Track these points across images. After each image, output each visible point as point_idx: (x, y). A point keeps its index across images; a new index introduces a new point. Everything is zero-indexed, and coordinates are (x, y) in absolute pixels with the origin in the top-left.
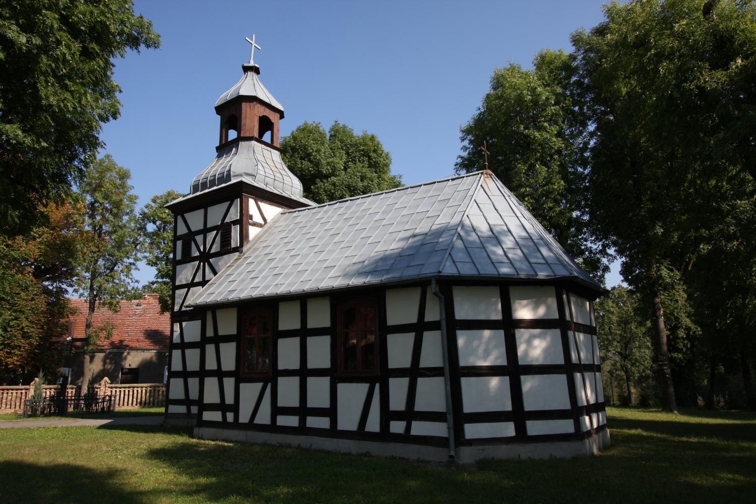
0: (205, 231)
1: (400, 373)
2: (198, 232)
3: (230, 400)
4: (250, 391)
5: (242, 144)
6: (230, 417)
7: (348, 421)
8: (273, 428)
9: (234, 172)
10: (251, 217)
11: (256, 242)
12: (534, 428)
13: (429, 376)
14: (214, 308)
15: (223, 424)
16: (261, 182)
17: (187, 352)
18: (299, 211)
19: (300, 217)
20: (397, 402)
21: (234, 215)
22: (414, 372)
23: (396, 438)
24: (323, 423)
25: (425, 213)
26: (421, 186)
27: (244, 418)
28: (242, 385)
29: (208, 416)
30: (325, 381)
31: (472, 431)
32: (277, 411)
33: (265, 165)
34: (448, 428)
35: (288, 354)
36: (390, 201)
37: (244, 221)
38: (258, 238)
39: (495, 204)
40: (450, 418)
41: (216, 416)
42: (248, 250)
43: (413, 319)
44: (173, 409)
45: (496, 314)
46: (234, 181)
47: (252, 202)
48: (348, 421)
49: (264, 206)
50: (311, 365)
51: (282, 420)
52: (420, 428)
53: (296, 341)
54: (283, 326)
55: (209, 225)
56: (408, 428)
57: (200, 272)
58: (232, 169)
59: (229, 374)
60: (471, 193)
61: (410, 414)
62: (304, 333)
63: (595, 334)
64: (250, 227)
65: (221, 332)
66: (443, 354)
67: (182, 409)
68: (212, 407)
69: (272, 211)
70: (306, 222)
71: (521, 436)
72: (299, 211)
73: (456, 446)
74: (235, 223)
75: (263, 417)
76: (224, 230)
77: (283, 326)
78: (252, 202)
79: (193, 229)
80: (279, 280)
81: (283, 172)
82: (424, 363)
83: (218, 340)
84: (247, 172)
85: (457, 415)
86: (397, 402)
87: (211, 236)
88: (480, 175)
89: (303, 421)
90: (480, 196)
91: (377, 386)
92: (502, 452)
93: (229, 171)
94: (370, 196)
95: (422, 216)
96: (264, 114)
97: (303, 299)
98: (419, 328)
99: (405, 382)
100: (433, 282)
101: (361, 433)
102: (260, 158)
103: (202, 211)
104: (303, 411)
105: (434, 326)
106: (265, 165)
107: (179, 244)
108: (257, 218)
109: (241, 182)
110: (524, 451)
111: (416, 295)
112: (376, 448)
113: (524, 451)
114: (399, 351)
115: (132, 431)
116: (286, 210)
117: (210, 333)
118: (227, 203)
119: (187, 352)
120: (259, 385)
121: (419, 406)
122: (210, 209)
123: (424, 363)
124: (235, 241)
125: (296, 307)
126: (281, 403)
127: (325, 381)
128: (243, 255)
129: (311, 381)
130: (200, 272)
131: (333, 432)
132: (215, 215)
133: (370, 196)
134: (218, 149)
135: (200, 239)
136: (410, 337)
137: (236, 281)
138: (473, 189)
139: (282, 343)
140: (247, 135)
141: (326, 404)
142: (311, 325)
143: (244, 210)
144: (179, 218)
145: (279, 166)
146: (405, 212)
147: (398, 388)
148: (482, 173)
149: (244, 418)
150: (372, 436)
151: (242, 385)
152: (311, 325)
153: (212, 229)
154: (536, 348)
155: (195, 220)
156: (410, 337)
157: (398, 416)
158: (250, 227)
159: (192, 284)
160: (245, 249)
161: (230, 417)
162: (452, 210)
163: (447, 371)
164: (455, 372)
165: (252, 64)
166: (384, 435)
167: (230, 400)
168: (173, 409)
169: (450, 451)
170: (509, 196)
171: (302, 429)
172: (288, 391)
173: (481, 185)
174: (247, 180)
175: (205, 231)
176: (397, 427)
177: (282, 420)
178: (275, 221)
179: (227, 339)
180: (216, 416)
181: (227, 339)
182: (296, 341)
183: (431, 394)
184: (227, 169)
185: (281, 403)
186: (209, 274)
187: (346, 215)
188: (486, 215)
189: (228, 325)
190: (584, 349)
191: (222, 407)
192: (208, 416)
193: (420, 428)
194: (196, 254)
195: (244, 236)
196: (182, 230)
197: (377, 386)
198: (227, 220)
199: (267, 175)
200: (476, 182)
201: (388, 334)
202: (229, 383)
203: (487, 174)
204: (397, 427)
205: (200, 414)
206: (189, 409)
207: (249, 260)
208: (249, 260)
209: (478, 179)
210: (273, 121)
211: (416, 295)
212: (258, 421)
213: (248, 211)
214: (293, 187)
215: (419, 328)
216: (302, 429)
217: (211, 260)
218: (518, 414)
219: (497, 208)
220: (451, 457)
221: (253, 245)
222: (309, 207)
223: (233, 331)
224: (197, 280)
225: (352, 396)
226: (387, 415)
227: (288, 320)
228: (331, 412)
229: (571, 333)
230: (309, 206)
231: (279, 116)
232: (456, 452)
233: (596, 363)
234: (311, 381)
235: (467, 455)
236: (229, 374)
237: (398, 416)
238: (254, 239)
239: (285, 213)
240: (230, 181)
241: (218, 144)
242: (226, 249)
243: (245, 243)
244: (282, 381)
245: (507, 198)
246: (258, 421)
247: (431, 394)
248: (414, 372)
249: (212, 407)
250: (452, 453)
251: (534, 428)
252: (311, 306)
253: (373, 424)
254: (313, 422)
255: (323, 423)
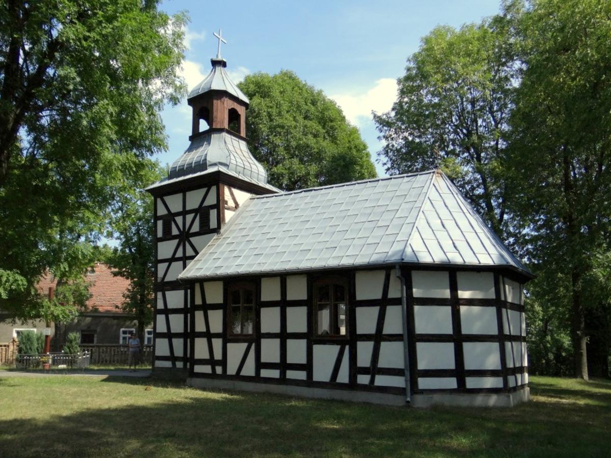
0: (184, 213)
1: (366, 337)
2: (178, 214)
3: (218, 356)
4: (236, 351)
5: (214, 137)
6: (219, 370)
7: (322, 373)
8: (257, 379)
9: (209, 161)
10: (226, 202)
11: (231, 225)
12: (471, 382)
13: (390, 341)
14: (202, 281)
15: (213, 375)
16: (233, 170)
17: (171, 317)
18: (266, 197)
19: (269, 203)
20: (364, 359)
21: (211, 200)
22: (378, 337)
23: (364, 388)
24: (301, 375)
25: (385, 207)
26: (379, 180)
27: (232, 370)
28: (229, 345)
29: (198, 369)
30: (303, 343)
31: (424, 383)
32: (260, 365)
33: (235, 155)
34: (406, 381)
35: (270, 320)
36: (353, 194)
37: (219, 206)
38: (233, 220)
39: (446, 201)
40: (407, 373)
41: (207, 369)
42: (226, 231)
43: (378, 295)
44: (159, 364)
45: (447, 294)
46: (210, 170)
47: (226, 190)
48: (322, 373)
49: (236, 192)
50: (290, 330)
51: (265, 373)
52: (381, 381)
53: (277, 310)
54: (265, 297)
55: (188, 208)
56: (372, 381)
57: (181, 249)
58: (208, 159)
59: (217, 336)
60: (425, 190)
61: (374, 370)
62: (284, 304)
63: (524, 311)
64: (226, 211)
65: (209, 301)
66: (403, 324)
67: (168, 364)
68: (202, 362)
69: (242, 196)
70: (276, 208)
71: (461, 388)
72: (266, 197)
73: (412, 394)
74: (212, 207)
75: (249, 369)
76: (203, 212)
77: (265, 297)
78: (226, 190)
79: (173, 211)
80: (238, 261)
81: (250, 161)
82: (387, 330)
83: (206, 307)
84: (221, 161)
85: (412, 371)
86: (364, 359)
87: (189, 217)
88: (432, 174)
89: (283, 374)
90: (432, 193)
91: (347, 347)
92: (447, 400)
93: (205, 159)
94: (333, 187)
95: (383, 209)
96: (233, 107)
97: (283, 277)
98: (383, 303)
99: (370, 345)
100: (397, 267)
101: (333, 383)
102: (231, 148)
103: (180, 196)
104: (283, 365)
105: (397, 302)
106: (235, 155)
107: (160, 223)
108: (231, 203)
109: (219, 172)
110: (463, 401)
111: (382, 276)
112: (345, 395)
113: (463, 401)
114: (366, 321)
115: (16, 420)
116: (254, 196)
117: (198, 301)
118: (205, 190)
119: (171, 317)
120: (245, 345)
121: (382, 364)
122: (188, 194)
123: (387, 330)
124: (213, 224)
125: (277, 282)
126: (264, 359)
127: (303, 343)
128: (222, 236)
129: (290, 343)
130: (181, 249)
131: (310, 382)
132: (194, 199)
133: (333, 187)
134: (191, 138)
135: (179, 220)
136: (376, 310)
137: (215, 259)
138: (426, 188)
139: (264, 312)
140: (218, 127)
141: (303, 360)
142: (290, 297)
143: (219, 195)
144: (159, 200)
145: (246, 154)
146: (368, 204)
147: (364, 351)
148: (434, 172)
149: (232, 370)
150: (342, 386)
151: (229, 345)
152: (290, 297)
153: (190, 212)
154: (478, 320)
155: (175, 203)
156: (376, 310)
157: (364, 371)
158: (226, 211)
159: (171, 261)
160: (222, 231)
161: (219, 370)
162: (409, 206)
163: (406, 337)
164: (411, 338)
165: (220, 58)
166: (352, 385)
167: (218, 356)
168: (159, 364)
169: (406, 398)
170: (457, 194)
171: (283, 380)
172: (270, 350)
173: (434, 184)
174: (223, 169)
175: (184, 213)
176: (364, 379)
177: (265, 373)
178: (246, 206)
179: (215, 307)
180: (207, 369)
181: (215, 307)
182: (277, 310)
183: (392, 355)
184: (203, 158)
185: (264, 359)
186: (190, 252)
187: (313, 204)
188: (438, 211)
189: (215, 295)
190: (515, 323)
191: (212, 362)
192: (198, 369)
193: (381, 381)
194: (175, 232)
195: (220, 219)
196: (162, 211)
197: (347, 347)
198: (206, 204)
199: (238, 164)
200: (429, 181)
201: (356, 307)
202: (217, 343)
203: (438, 173)
204: (364, 379)
205: (192, 368)
206: (174, 364)
207: (229, 241)
208: (229, 241)
209: (430, 177)
210: (240, 113)
211: (382, 276)
212: (244, 373)
213: (223, 197)
214: (258, 173)
215: (383, 303)
216: (283, 380)
217: (190, 239)
218: (460, 372)
219: (447, 204)
220: (408, 402)
221: (229, 227)
222: (276, 194)
223: (220, 300)
224: (177, 256)
225: (325, 356)
226: (355, 370)
227: (270, 291)
228: (308, 367)
229: (504, 310)
230: (276, 192)
231: (244, 108)
232: (411, 398)
233: (523, 335)
234: (290, 343)
235: (420, 401)
236: (217, 336)
237: (364, 371)
238: (229, 221)
239: (254, 199)
240: (206, 169)
241: (191, 134)
242: (206, 230)
243: (222, 225)
244: (264, 342)
245: (456, 196)
246: (243, 373)
247: (392, 355)
248: (378, 337)
249: (202, 362)
250: (409, 399)
251: (471, 382)
252: (290, 282)
253: (343, 376)
254: (291, 374)
255: (301, 375)
